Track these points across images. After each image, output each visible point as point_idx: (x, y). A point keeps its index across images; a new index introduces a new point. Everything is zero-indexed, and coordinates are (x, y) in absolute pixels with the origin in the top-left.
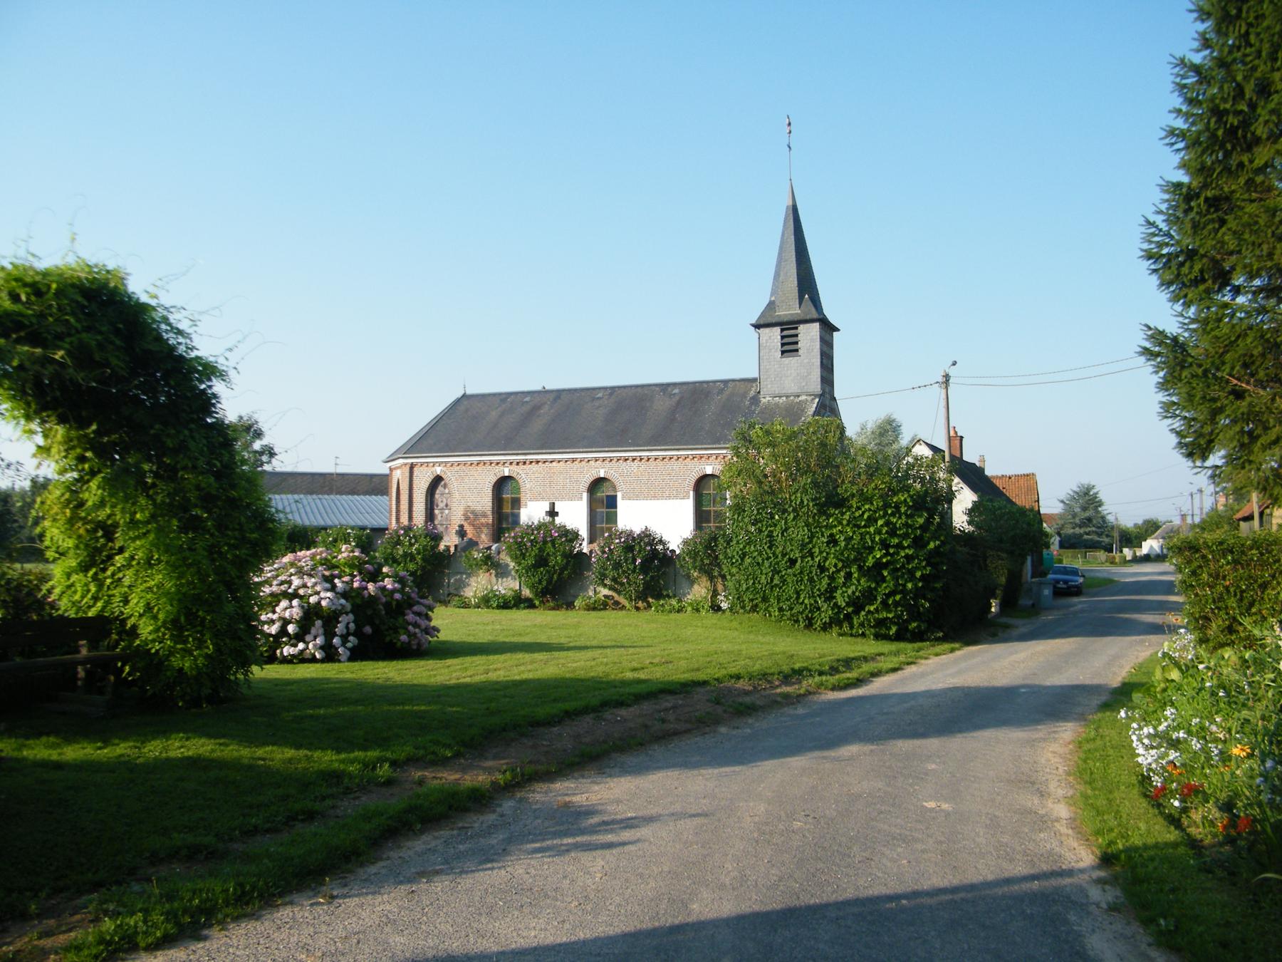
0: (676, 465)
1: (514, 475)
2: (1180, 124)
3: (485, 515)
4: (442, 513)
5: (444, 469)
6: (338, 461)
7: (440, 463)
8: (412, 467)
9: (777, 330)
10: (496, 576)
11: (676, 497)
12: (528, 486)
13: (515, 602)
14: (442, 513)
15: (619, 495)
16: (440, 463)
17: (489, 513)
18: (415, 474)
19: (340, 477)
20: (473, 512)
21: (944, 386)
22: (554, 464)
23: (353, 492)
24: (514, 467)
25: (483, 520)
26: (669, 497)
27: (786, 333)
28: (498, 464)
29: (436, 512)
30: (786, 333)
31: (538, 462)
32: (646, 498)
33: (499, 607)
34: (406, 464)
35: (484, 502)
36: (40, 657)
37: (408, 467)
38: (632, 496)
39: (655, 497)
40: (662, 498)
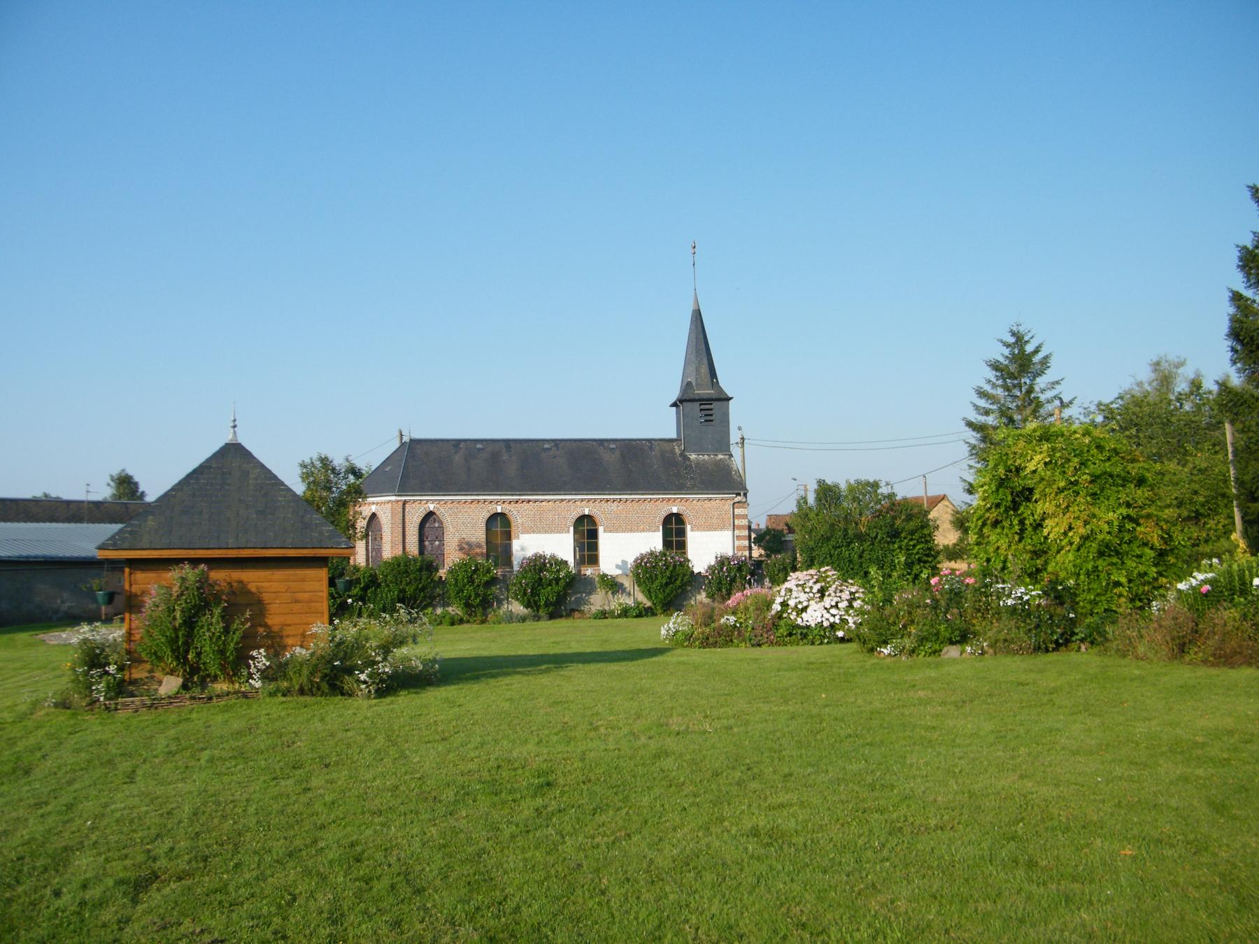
0: (648, 506)
1: (506, 512)
2: (1181, 386)
3: (479, 546)
4: (432, 544)
5: (438, 506)
6: (90, 489)
7: (433, 501)
8: (405, 503)
9: (697, 404)
10: (613, 593)
11: (649, 530)
12: (520, 521)
13: (643, 612)
14: (432, 544)
15: (601, 529)
16: (433, 501)
17: (484, 544)
18: (407, 510)
19: (33, 503)
20: (467, 543)
21: (740, 445)
22: (544, 503)
23: (53, 519)
24: (506, 505)
25: (478, 550)
26: (643, 531)
27: (703, 407)
28: (491, 502)
29: (427, 543)
30: (703, 407)
31: (529, 501)
32: (624, 531)
33: (637, 616)
34: (398, 501)
35: (478, 535)
36: (519, 667)
37: (401, 504)
38: (609, 530)
39: (631, 531)
40: (637, 531)
